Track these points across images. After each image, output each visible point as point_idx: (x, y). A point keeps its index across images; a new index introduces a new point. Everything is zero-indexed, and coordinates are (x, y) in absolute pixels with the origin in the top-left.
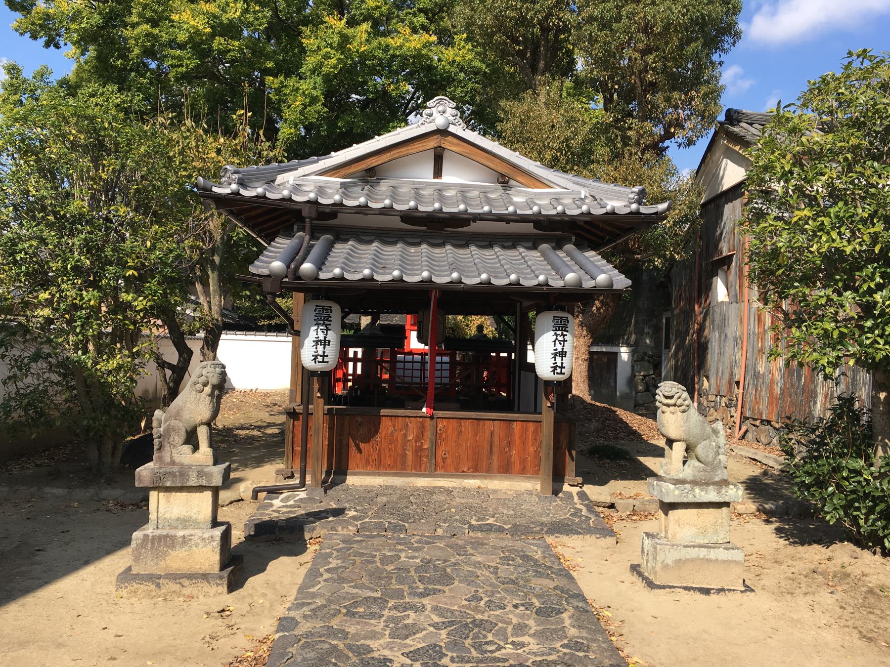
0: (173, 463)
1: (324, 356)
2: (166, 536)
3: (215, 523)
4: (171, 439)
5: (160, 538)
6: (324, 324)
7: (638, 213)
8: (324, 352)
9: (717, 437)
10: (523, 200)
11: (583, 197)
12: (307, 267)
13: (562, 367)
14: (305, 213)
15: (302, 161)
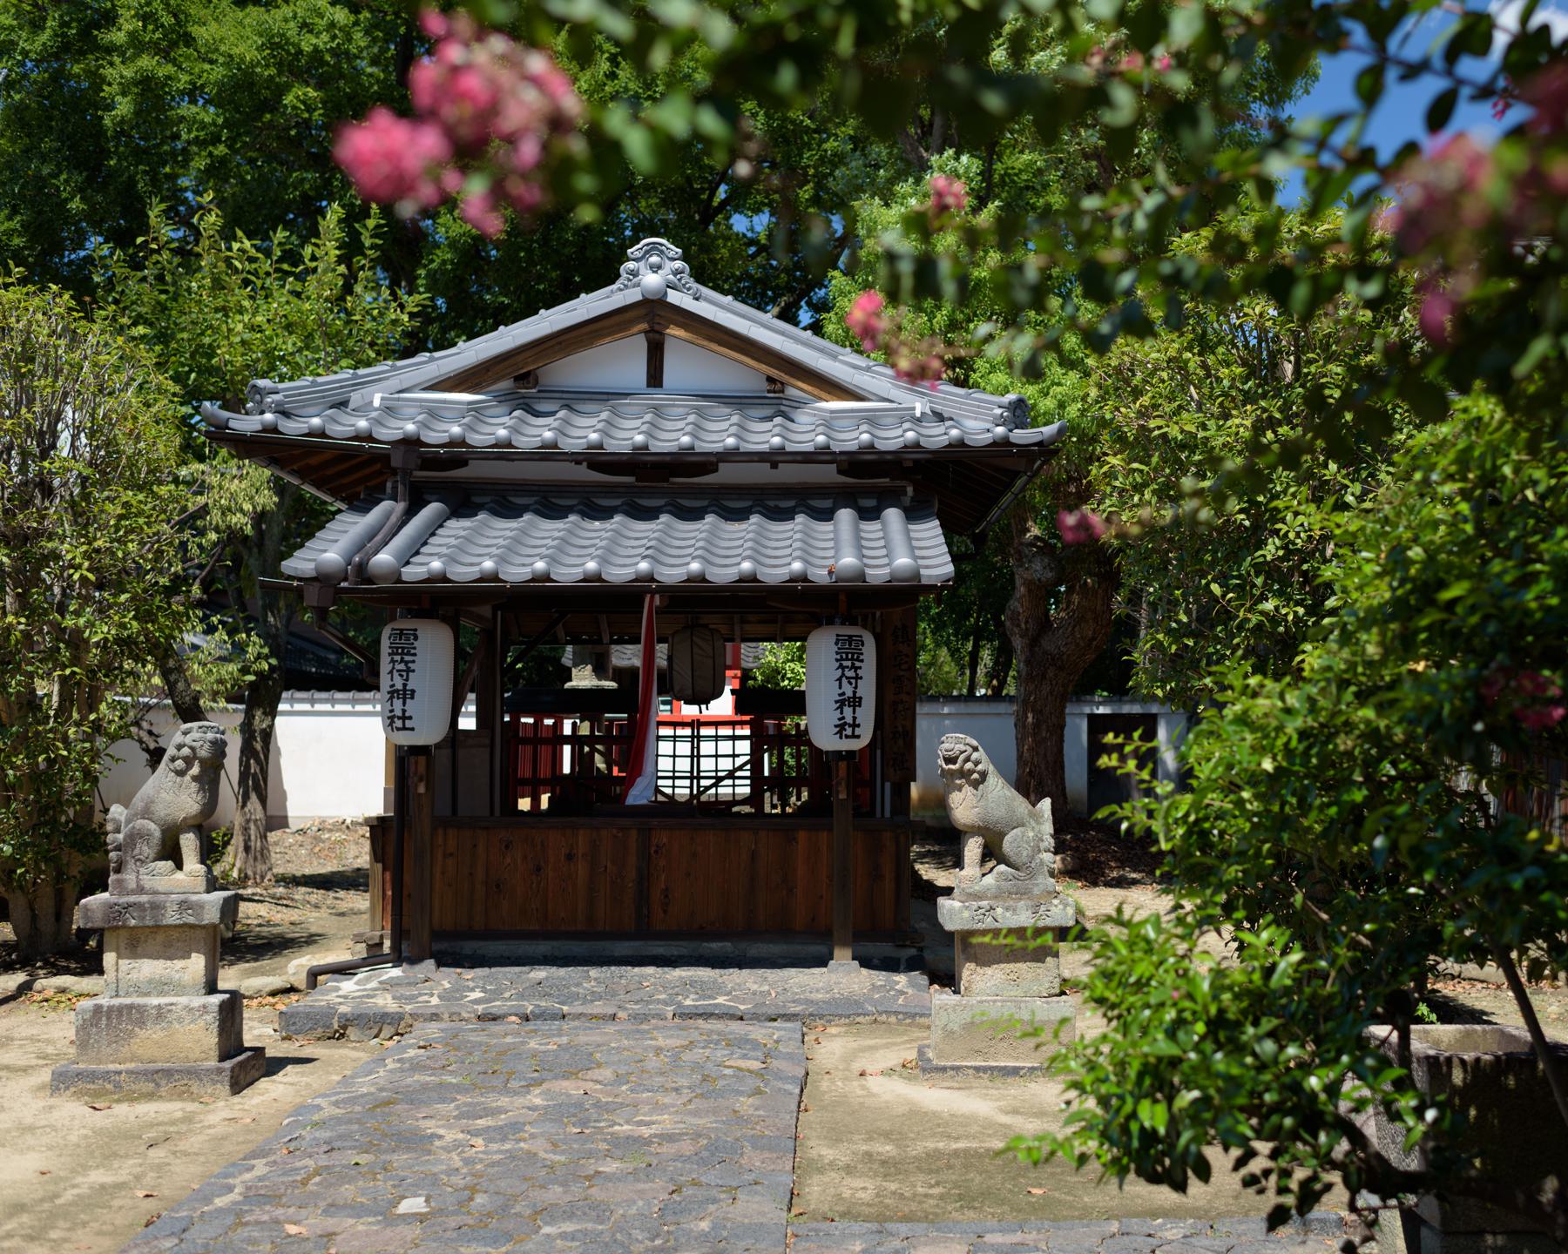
0: (141, 890)
1: (404, 718)
2: (131, 1007)
3: (211, 988)
4: (137, 851)
5: (120, 1009)
6: (402, 661)
7: (1005, 442)
8: (404, 711)
9: (1038, 823)
10: (814, 425)
11: (918, 414)
12: (384, 558)
13: (855, 725)
14: (396, 462)
15: (400, 363)
